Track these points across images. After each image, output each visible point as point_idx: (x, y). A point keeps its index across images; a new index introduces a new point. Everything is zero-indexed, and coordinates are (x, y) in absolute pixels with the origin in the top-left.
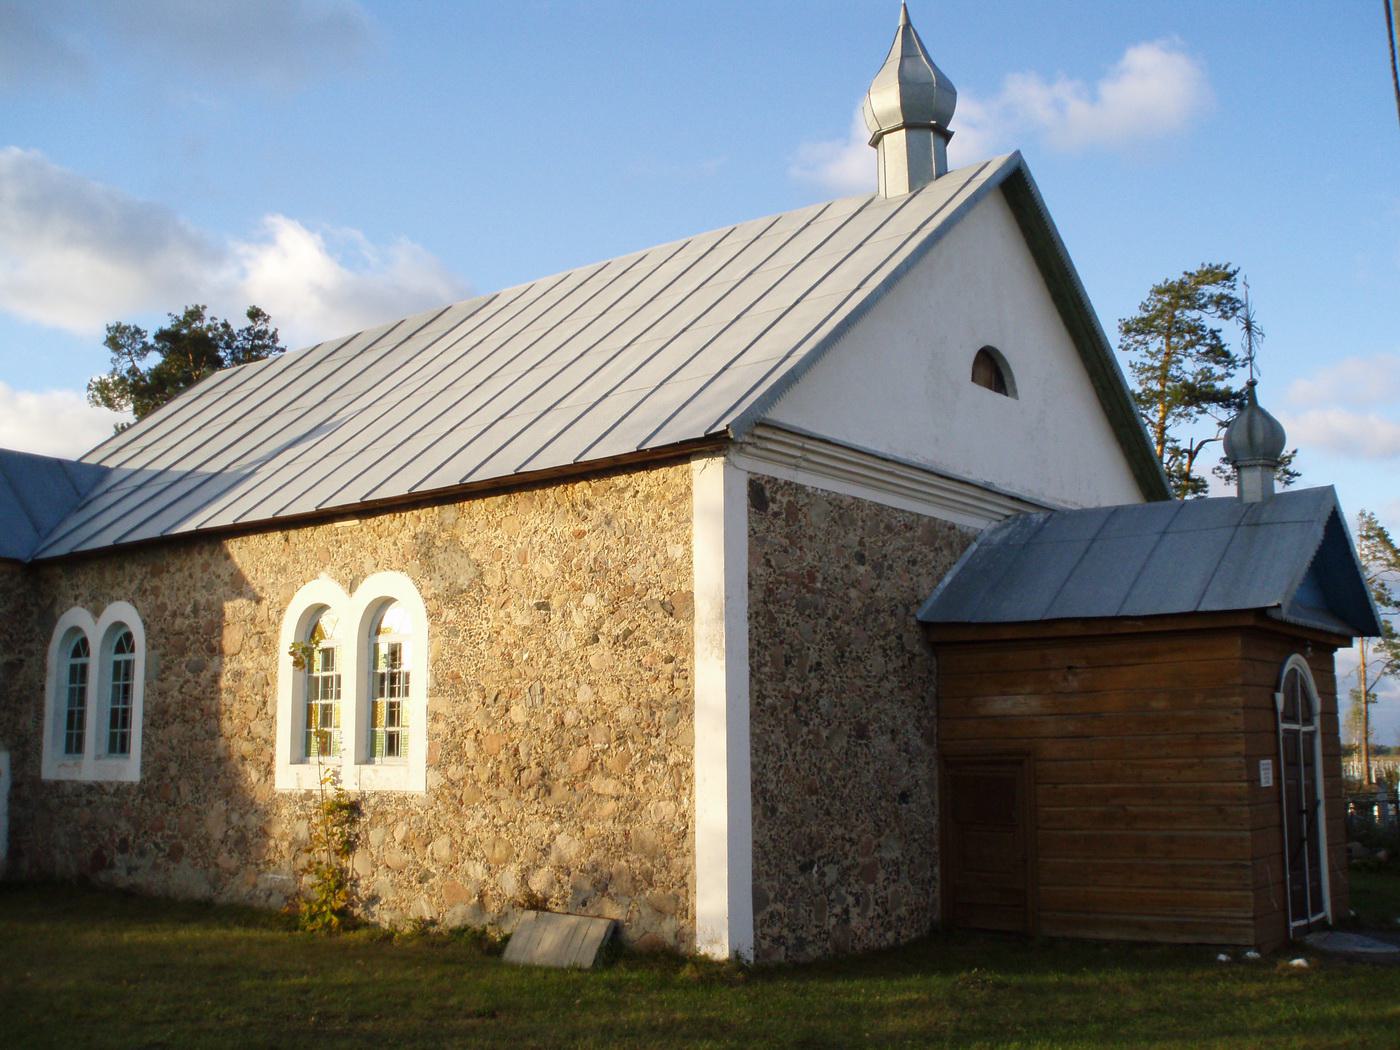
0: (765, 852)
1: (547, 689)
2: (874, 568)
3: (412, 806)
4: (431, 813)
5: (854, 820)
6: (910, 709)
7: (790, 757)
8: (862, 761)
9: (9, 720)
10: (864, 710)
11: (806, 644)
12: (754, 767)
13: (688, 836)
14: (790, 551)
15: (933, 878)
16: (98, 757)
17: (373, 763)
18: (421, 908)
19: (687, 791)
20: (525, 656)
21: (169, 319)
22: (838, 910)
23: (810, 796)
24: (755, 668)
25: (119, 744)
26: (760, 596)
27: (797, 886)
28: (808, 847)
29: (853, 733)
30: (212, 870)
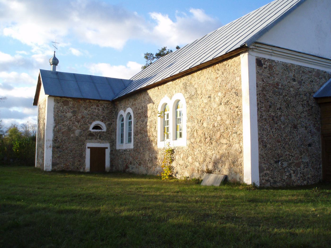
0: (263, 157)
1: (211, 118)
2: (299, 83)
3: (184, 149)
4: (188, 151)
5: (292, 150)
6: (312, 121)
7: (271, 132)
8: (295, 134)
9: (109, 136)
10: (296, 121)
11: (276, 102)
12: (259, 134)
13: (242, 152)
14: (270, 77)
15: (320, 168)
16: (126, 144)
17: (177, 140)
18: (186, 174)
19: (242, 141)
20: (206, 110)
21: (158, 51)
22: (288, 174)
23: (278, 143)
24: (259, 108)
25: (130, 141)
26: (261, 89)
27: (274, 167)
28: (277, 156)
29: (292, 127)
30: (147, 167)
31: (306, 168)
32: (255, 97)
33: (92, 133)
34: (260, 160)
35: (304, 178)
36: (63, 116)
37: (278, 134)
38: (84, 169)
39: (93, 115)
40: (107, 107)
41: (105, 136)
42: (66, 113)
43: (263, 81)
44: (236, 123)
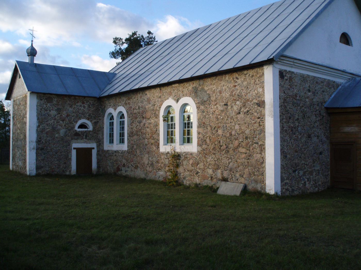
0: (284, 167)
2: (313, 93)
3: (194, 155)
5: (307, 159)
6: (323, 130)
7: (290, 143)
10: (310, 131)
12: (281, 145)
14: (290, 89)
16: (117, 144)
21: (128, 35)
22: (303, 182)
24: (281, 120)
26: (282, 101)
27: (292, 176)
28: (295, 166)
30: (145, 171)
31: (318, 175)
32: (278, 109)
33: (78, 132)
34: (281, 171)
35: (316, 185)
36: (47, 115)
37: (296, 144)
38: (70, 171)
39: (78, 113)
40: (93, 104)
41: (92, 136)
42: (50, 111)
43: (284, 93)
44: (257, 134)
